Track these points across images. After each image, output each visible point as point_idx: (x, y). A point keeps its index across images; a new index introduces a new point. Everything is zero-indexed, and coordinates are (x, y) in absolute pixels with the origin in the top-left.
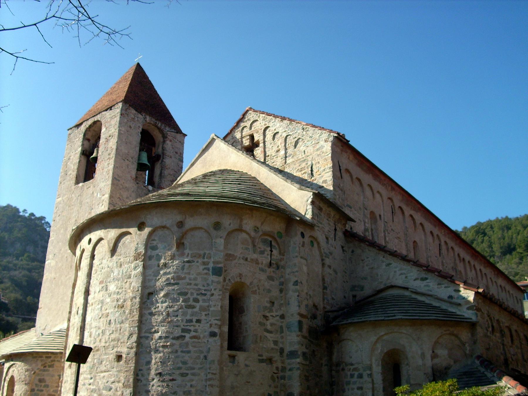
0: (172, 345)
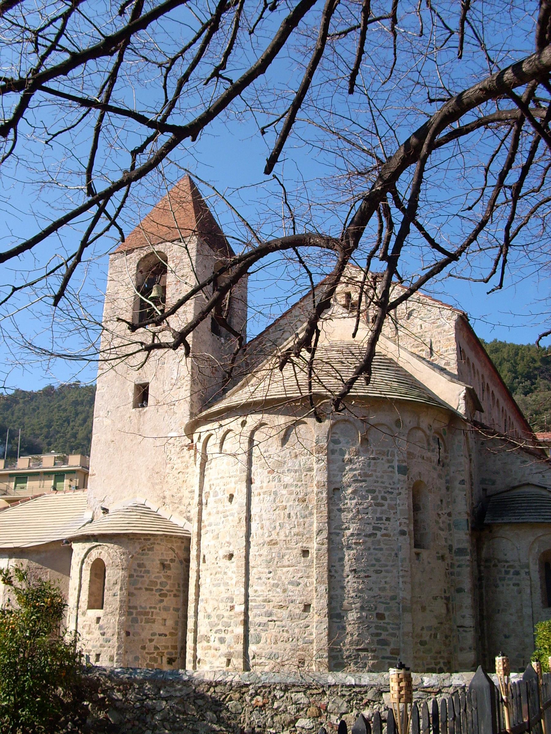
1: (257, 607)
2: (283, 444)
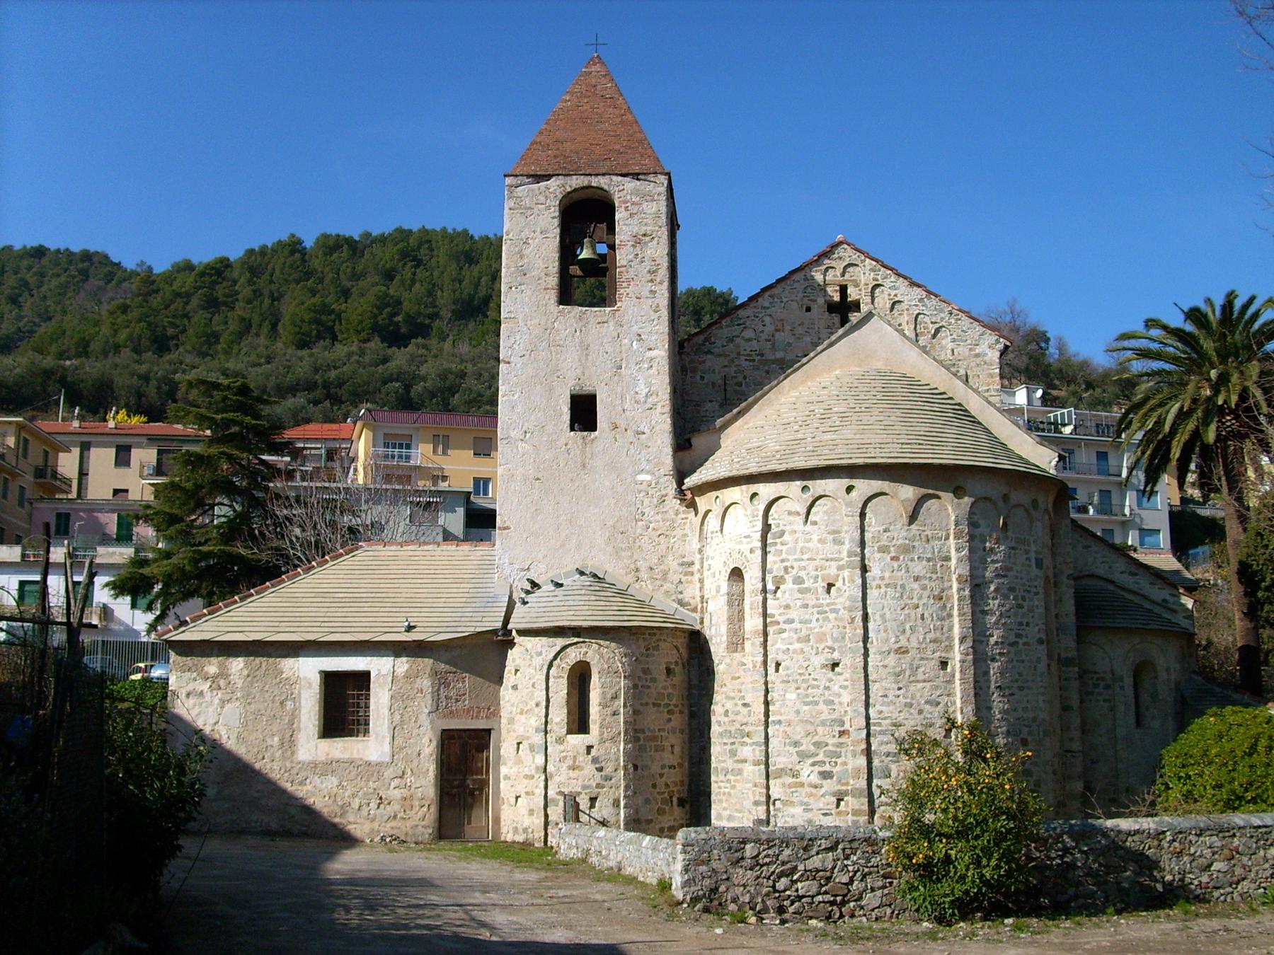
0: (1009, 652)
1: (883, 733)
2: (911, 523)
